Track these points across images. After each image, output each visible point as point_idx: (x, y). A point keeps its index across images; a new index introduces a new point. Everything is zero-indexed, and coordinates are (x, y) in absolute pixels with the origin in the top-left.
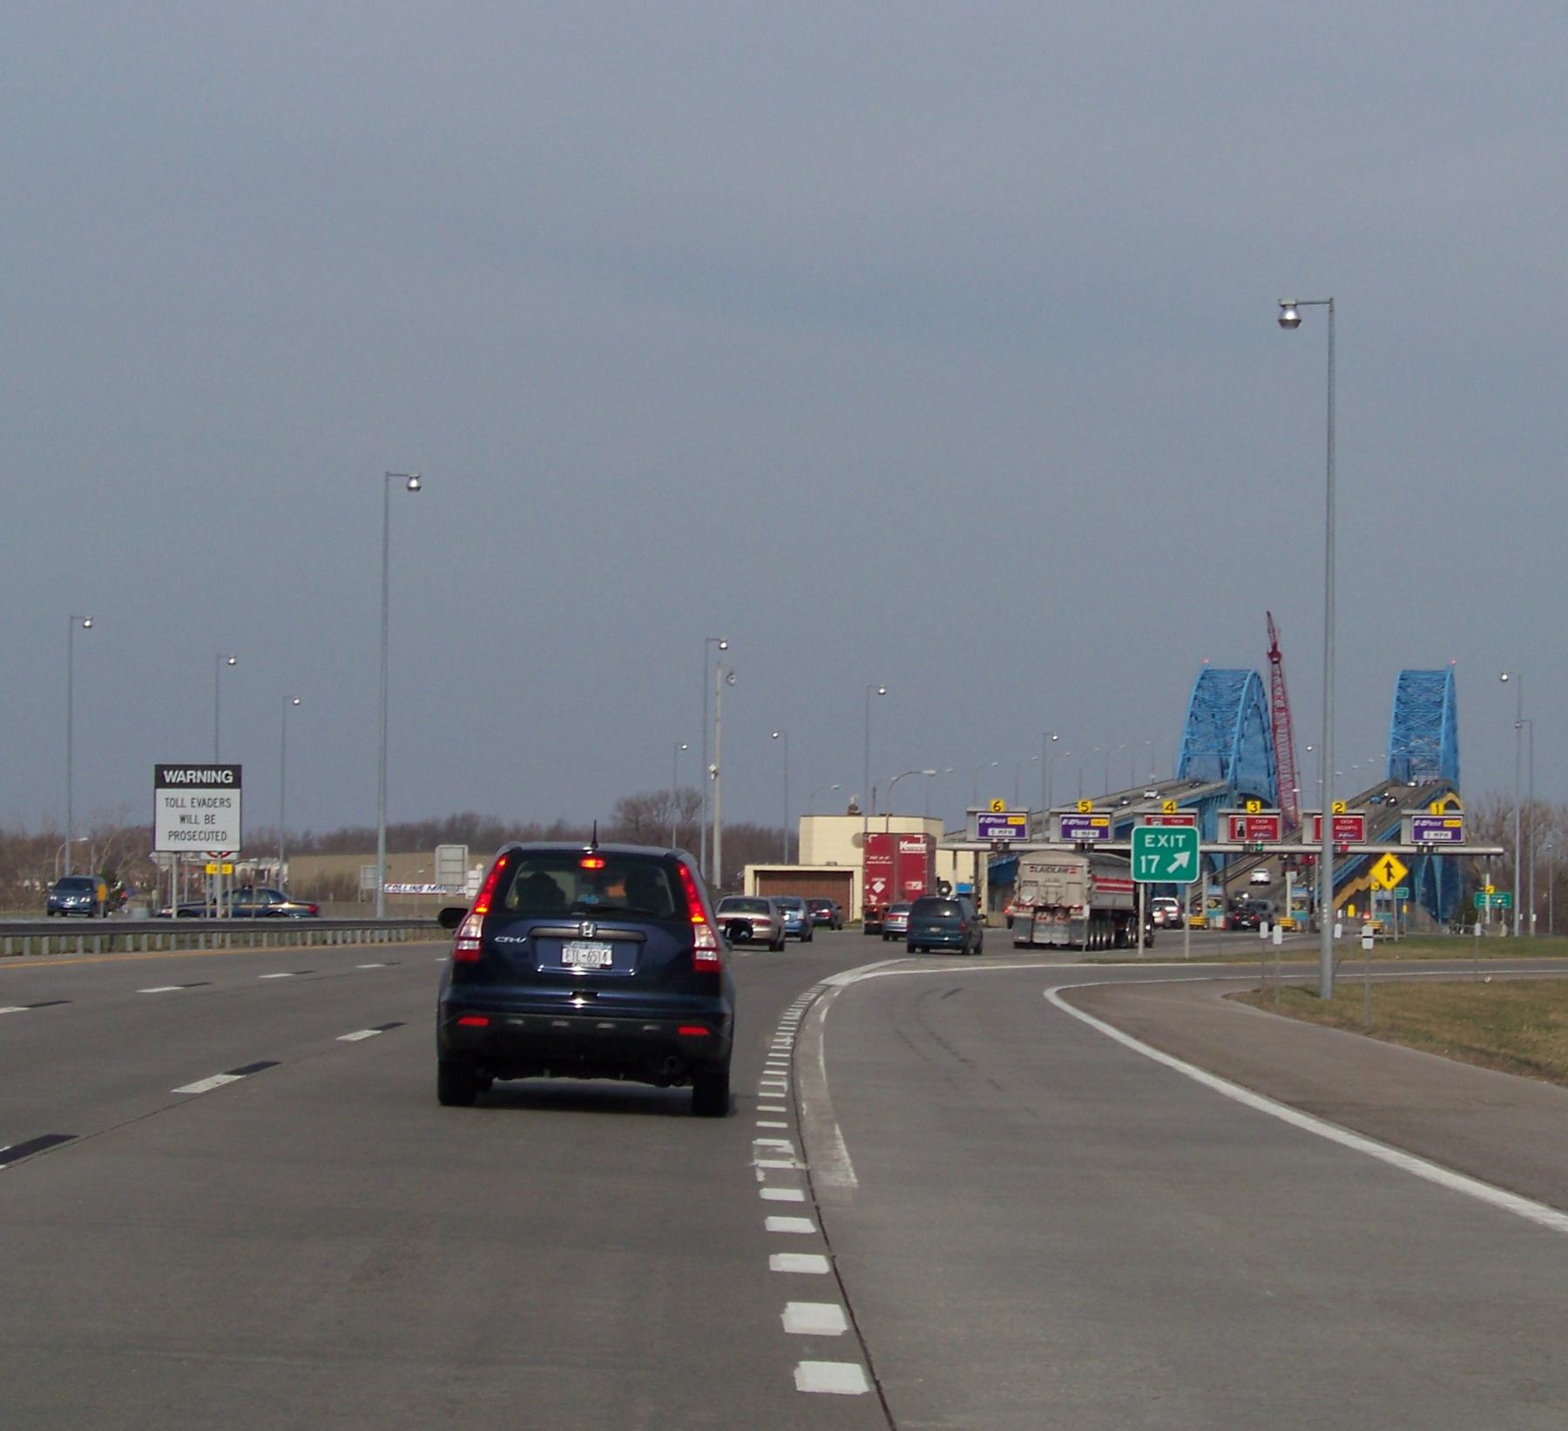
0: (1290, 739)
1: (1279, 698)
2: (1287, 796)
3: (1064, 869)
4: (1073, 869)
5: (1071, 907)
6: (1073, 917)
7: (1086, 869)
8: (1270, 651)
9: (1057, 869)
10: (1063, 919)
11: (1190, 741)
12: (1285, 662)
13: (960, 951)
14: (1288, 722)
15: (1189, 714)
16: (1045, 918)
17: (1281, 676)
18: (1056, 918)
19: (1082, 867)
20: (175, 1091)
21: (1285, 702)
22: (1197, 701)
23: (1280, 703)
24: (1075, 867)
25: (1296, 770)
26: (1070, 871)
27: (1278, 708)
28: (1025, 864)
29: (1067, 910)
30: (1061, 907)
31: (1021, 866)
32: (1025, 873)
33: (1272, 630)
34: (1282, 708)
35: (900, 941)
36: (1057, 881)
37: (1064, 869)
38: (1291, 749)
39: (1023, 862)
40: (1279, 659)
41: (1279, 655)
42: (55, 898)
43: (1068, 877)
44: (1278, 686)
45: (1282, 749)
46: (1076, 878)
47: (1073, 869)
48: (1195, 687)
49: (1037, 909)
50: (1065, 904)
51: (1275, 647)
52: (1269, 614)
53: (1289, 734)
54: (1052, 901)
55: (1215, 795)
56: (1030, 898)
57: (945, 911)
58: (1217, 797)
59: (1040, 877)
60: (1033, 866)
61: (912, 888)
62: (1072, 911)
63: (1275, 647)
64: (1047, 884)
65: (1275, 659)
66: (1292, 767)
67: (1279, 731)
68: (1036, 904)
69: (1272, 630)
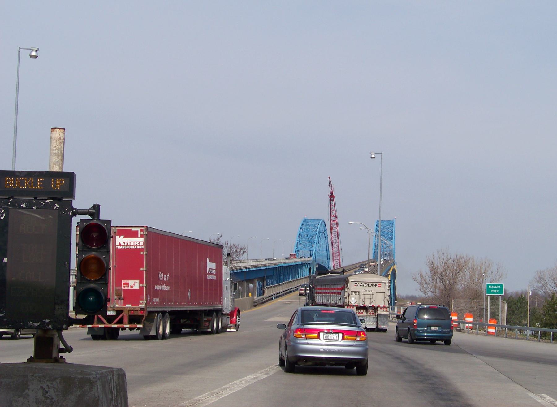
0: (338, 234)
1: (334, 216)
2: (335, 259)
3: (374, 284)
4: (379, 284)
5: (379, 307)
6: (379, 313)
7: (387, 284)
8: (330, 195)
9: (370, 284)
10: (373, 314)
11: (298, 244)
12: (336, 199)
13: (221, 298)
14: (337, 226)
15: (298, 234)
16: (362, 313)
17: (334, 206)
18: (369, 313)
19: (385, 283)
20: (189, 290)
21: (336, 218)
22: (302, 229)
23: (333, 218)
24: (380, 283)
25: (340, 248)
26: (377, 285)
27: (333, 221)
28: (352, 281)
29: (375, 309)
30: (373, 307)
31: (350, 282)
32: (352, 287)
33: (330, 186)
34: (334, 221)
35: (459, 350)
36: (371, 291)
37: (374, 284)
38: (338, 238)
39: (350, 280)
40: (334, 199)
41: (334, 197)
42: (311, 287)
43: (377, 289)
44: (333, 210)
45: (334, 238)
46: (382, 289)
47: (379, 284)
48: (301, 224)
49: (359, 308)
50: (376, 305)
51: (332, 193)
52: (329, 178)
53: (338, 232)
54: (367, 303)
55: (307, 263)
56: (355, 301)
57: (424, 315)
58: (308, 264)
59: (361, 289)
60: (356, 283)
61: (130, 288)
62: (379, 309)
63: (332, 193)
64: (365, 293)
65: (332, 199)
66: (339, 246)
67: (333, 230)
68: (358, 305)
69: (330, 186)
